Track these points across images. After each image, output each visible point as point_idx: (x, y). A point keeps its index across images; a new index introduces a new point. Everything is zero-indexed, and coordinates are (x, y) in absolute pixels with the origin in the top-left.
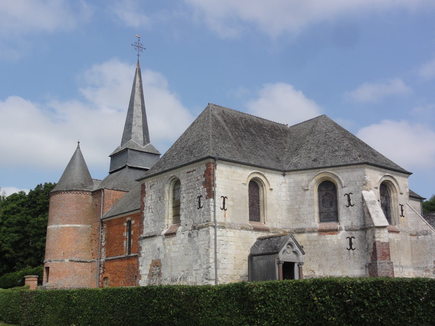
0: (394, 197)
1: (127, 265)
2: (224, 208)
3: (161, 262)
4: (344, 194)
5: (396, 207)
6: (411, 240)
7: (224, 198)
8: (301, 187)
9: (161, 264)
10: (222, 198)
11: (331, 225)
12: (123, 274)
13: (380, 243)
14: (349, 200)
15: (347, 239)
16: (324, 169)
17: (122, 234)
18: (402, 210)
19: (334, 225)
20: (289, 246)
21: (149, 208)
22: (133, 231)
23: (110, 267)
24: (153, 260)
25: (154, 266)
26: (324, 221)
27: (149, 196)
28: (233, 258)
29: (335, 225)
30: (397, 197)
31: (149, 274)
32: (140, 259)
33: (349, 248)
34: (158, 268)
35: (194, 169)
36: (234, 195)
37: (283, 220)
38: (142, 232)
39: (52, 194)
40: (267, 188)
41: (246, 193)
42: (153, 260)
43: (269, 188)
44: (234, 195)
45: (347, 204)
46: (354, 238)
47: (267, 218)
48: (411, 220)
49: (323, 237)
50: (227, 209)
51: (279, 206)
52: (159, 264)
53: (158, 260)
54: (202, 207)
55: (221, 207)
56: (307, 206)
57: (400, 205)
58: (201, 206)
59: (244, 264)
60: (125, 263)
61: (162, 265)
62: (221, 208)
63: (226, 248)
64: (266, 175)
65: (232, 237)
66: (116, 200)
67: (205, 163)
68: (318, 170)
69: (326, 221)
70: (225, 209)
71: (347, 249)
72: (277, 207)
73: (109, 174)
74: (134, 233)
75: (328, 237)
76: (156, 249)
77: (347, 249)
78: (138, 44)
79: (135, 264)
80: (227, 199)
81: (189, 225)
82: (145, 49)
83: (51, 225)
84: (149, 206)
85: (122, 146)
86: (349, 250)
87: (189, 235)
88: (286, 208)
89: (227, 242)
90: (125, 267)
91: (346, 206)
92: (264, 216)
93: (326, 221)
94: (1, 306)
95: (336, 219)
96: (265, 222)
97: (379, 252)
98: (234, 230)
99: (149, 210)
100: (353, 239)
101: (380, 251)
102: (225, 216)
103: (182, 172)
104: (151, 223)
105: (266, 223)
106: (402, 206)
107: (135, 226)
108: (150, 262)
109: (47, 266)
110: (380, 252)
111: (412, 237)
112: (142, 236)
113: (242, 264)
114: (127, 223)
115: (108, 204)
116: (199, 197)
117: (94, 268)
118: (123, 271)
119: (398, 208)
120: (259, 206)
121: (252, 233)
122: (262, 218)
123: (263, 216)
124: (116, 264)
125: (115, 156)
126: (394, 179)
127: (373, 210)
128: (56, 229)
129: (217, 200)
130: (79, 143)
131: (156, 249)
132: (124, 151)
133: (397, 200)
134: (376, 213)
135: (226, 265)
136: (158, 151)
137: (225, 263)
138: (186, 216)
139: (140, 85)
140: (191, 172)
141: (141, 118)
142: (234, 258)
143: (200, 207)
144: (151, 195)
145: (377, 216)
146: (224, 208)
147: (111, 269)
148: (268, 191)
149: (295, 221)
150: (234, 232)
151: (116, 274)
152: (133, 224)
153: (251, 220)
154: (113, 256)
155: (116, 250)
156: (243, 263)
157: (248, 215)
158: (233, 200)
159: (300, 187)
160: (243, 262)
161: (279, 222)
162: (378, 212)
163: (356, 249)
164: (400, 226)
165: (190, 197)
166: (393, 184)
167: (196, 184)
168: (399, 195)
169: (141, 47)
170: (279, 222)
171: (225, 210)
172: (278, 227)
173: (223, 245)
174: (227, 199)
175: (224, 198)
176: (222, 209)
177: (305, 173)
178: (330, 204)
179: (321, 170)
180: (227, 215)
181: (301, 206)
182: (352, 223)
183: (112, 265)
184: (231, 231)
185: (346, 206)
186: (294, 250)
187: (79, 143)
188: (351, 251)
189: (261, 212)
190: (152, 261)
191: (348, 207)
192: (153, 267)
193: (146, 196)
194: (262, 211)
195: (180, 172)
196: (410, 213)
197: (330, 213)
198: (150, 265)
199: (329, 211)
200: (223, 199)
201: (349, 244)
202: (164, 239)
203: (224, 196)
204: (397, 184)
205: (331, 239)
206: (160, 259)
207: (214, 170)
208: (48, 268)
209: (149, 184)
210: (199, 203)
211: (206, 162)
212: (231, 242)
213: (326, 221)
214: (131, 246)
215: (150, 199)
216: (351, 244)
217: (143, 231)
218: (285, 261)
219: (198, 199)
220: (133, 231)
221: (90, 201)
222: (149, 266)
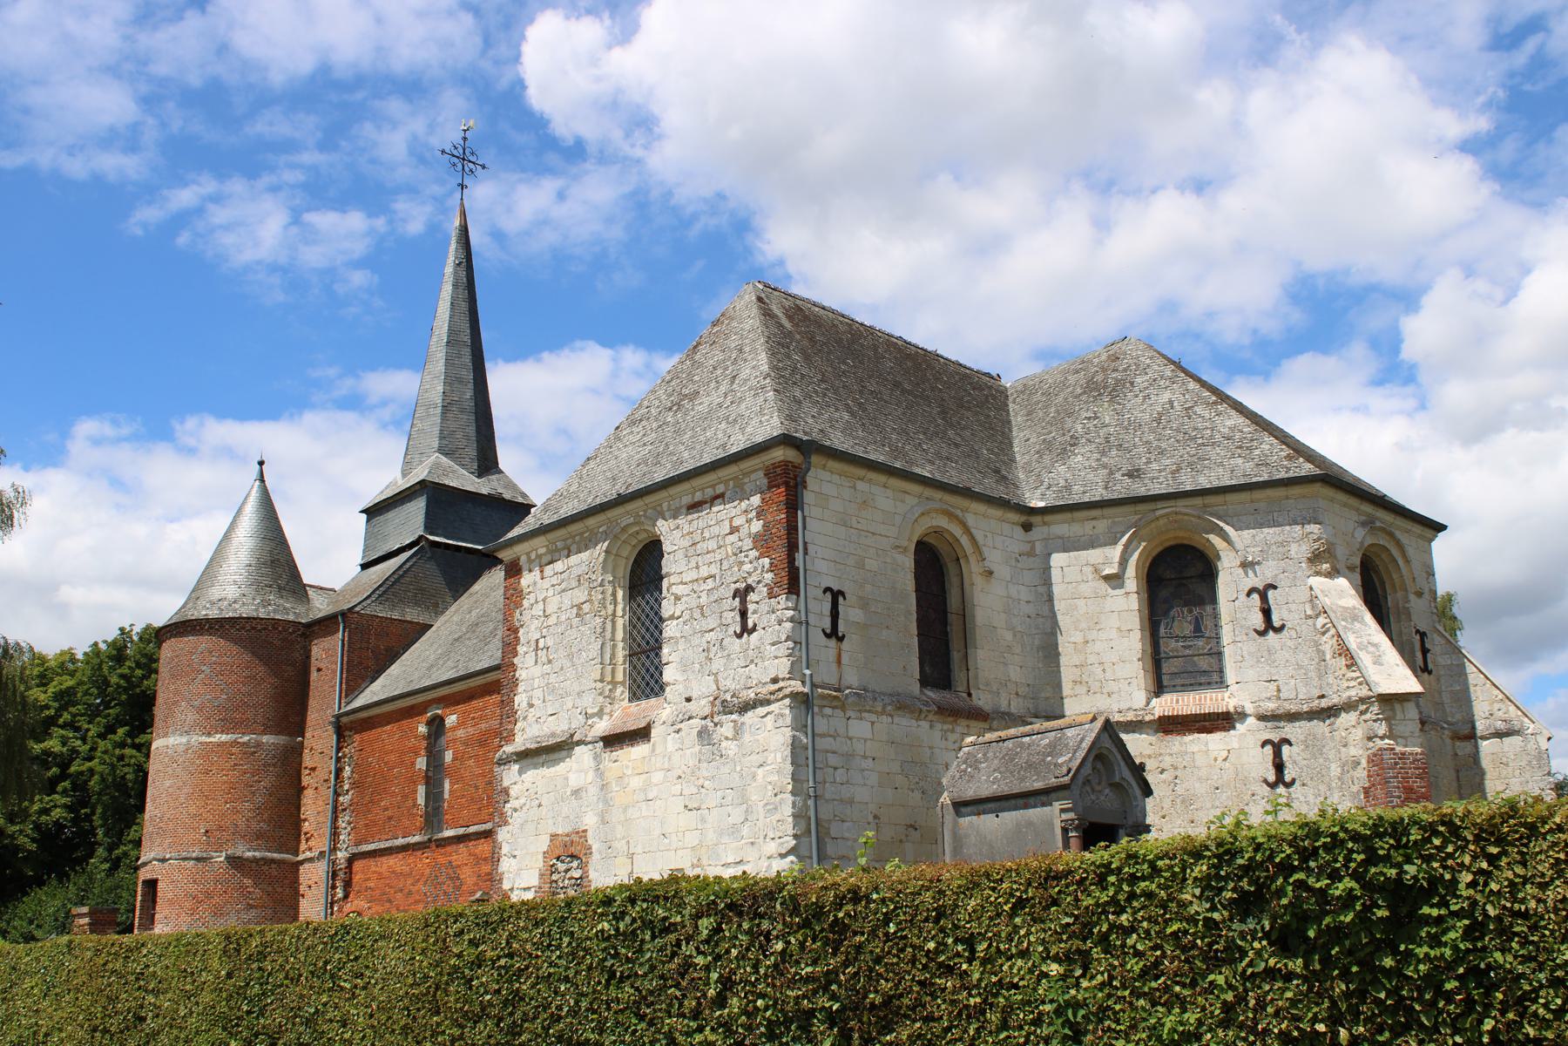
0: (1398, 604)
1: (428, 871)
2: (833, 633)
3: (590, 842)
4: (1246, 590)
5: (1405, 638)
6: (1456, 754)
7: (836, 595)
8: (1090, 569)
9: (590, 848)
10: (829, 595)
11: (1200, 700)
12: (417, 902)
13: (1394, 754)
14: (1267, 612)
15: (1263, 746)
16: (1172, 503)
17: (413, 764)
18: (1425, 651)
19: (1211, 699)
20: (1099, 766)
21: (537, 649)
22: (451, 752)
23: (369, 879)
24: (554, 836)
25: (558, 859)
26: (1174, 686)
27: (537, 602)
28: (871, 819)
29: (1217, 700)
30: (1407, 605)
31: (540, 888)
32: (502, 835)
33: (1272, 778)
34: (575, 864)
35: (718, 492)
36: (868, 587)
37: (1028, 685)
38: (510, 738)
39: (169, 631)
40: (973, 569)
41: (908, 583)
42: (554, 836)
43: (981, 570)
44: (868, 587)
45: (1260, 625)
46: (1291, 744)
47: (976, 677)
48: (1452, 685)
49: (1177, 743)
50: (844, 636)
51: (1015, 635)
52: (579, 848)
53: (578, 833)
54: (754, 629)
55: (825, 627)
56: (1114, 634)
57: (1418, 631)
58: (750, 624)
59: (908, 841)
60: (423, 861)
61: (591, 853)
62: (823, 630)
63: (848, 782)
64: (971, 520)
65: (865, 740)
66: (387, 651)
67: (761, 465)
68: (1151, 506)
69: (1183, 685)
70: (840, 634)
71: (1265, 781)
72: (1008, 636)
73: (359, 568)
74: (455, 759)
75: (1196, 743)
76: (568, 793)
77: (1265, 781)
78: (461, 151)
79: (459, 866)
80: (845, 599)
81: (699, 698)
82: (483, 167)
83: (166, 735)
84: (537, 641)
85: (404, 474)
86: (1273, 786)
87: (703, 734)
88: (1037, 642)
89: (849, 756)
90: (423, 874)
91: (1256, 631)
92: (968, 670)
93: (1179, 688)
94: (845, 1035)
95: (1213, 677)
96: (972, 692)
97: (1395, 787)
98: (873, 717)
99: (537, 655)
100: (1285, 749)
101: (1399, 782)
102: (839, 662)
103: (669, 505)
104: (544, 701)
105: (974, 696)
106: (1423, 635)
107: (460, 733)
108: (544, 843)
109: (149, 877)
110: (1398, 787)
111: (1458, 743)
112: (508, 749)
113: (901, 841)
114: (429, 723)
115: (361, 663)
116: (743, 594)
117: (310, 883)
118: (414, 889)
119: (1412, 643)
120: (946, 634)
121: (931, 727)
122: (958, 676)
123: (964, 668)
124: (390, 867)
125: (381, 508)
126: (1398, 544)
127: (1358, 640)
128: (182, 748)
129: (812, 605)
130: (261, 463)
131: (565, 792)
132: (413, 490)
133: (1409, 615)
134: (1371, 649)
135: (850, 843)
136: (524, 495)
137: (847, 835)
138: (685, 667)
139: (468, 280)
140: (706, 502)
141: (471, 386)
142: (875, 817)
143: (746, 630)
144: (544, 600)
145: (1377, 661)
146: (833, 633)
147: (372, 885)
148: (979, 581)
149: (1073, 689)
150: (873, 723)
151: (390, 901)
152: (454, 729)
153: (925, 682)
154: (380, 840)
155: (390, 818)
156: (903, 838)
157: (917, 661)
158: (864, 604)
159: (1084, 568)
160: (907, 836)
161: (1017, 694)
162: (1375, 645)
163: (1297, 783)
164: (1421, 703)
165: (704, 595)
166: (1394, 560)
167: (725, 546)
168: (1412, 597)
169: (470, 161)
170: (1017, 694)
171: (841, 639)
172: (1013, 710)
173: (835, 768)
174: (845, 599)
175: (836, 595)
176: (828, 636)
177: (1103, 517)
178: (1192, 627)
179: (1160, 505)
180: (845, 659)
181: (1093, 635)
182: (1279, 690)
183: (375, 872)
184: (861, 719)
185: (1256, 631)
186: (1117, 779)
187: (261, 463)
188: (1281, 790)
189: (956, 656)
190: (551, 841)
191: (1262, 633)
192: (555, 861)
193: (526, 603)
194: (959, 651)
195: (659, 508)
196: (1449, 662)
197: (1196, 658)
198: (544, 853)
199: (1191, 652)
200: (830, 600)
201: (1271, 764)
202: (596, 757)
203: (835, 589)
204: (1407, 561)
205: (1204, 749)
206: (585, 831)
207: (796, 492)
208: (152, 885)
209: (534, 560)
210: (743, 614)
211: (767, 464)
212: (865, 757)
213: (1183, 685)
214: (446, 804)
215: (541, 613)
216: (1279, 767)
217: (513, 730)
218: (1094, 820)
219: (737, 599)
220: (451, 752)
221: (298, 655)
222: (541, 857)
